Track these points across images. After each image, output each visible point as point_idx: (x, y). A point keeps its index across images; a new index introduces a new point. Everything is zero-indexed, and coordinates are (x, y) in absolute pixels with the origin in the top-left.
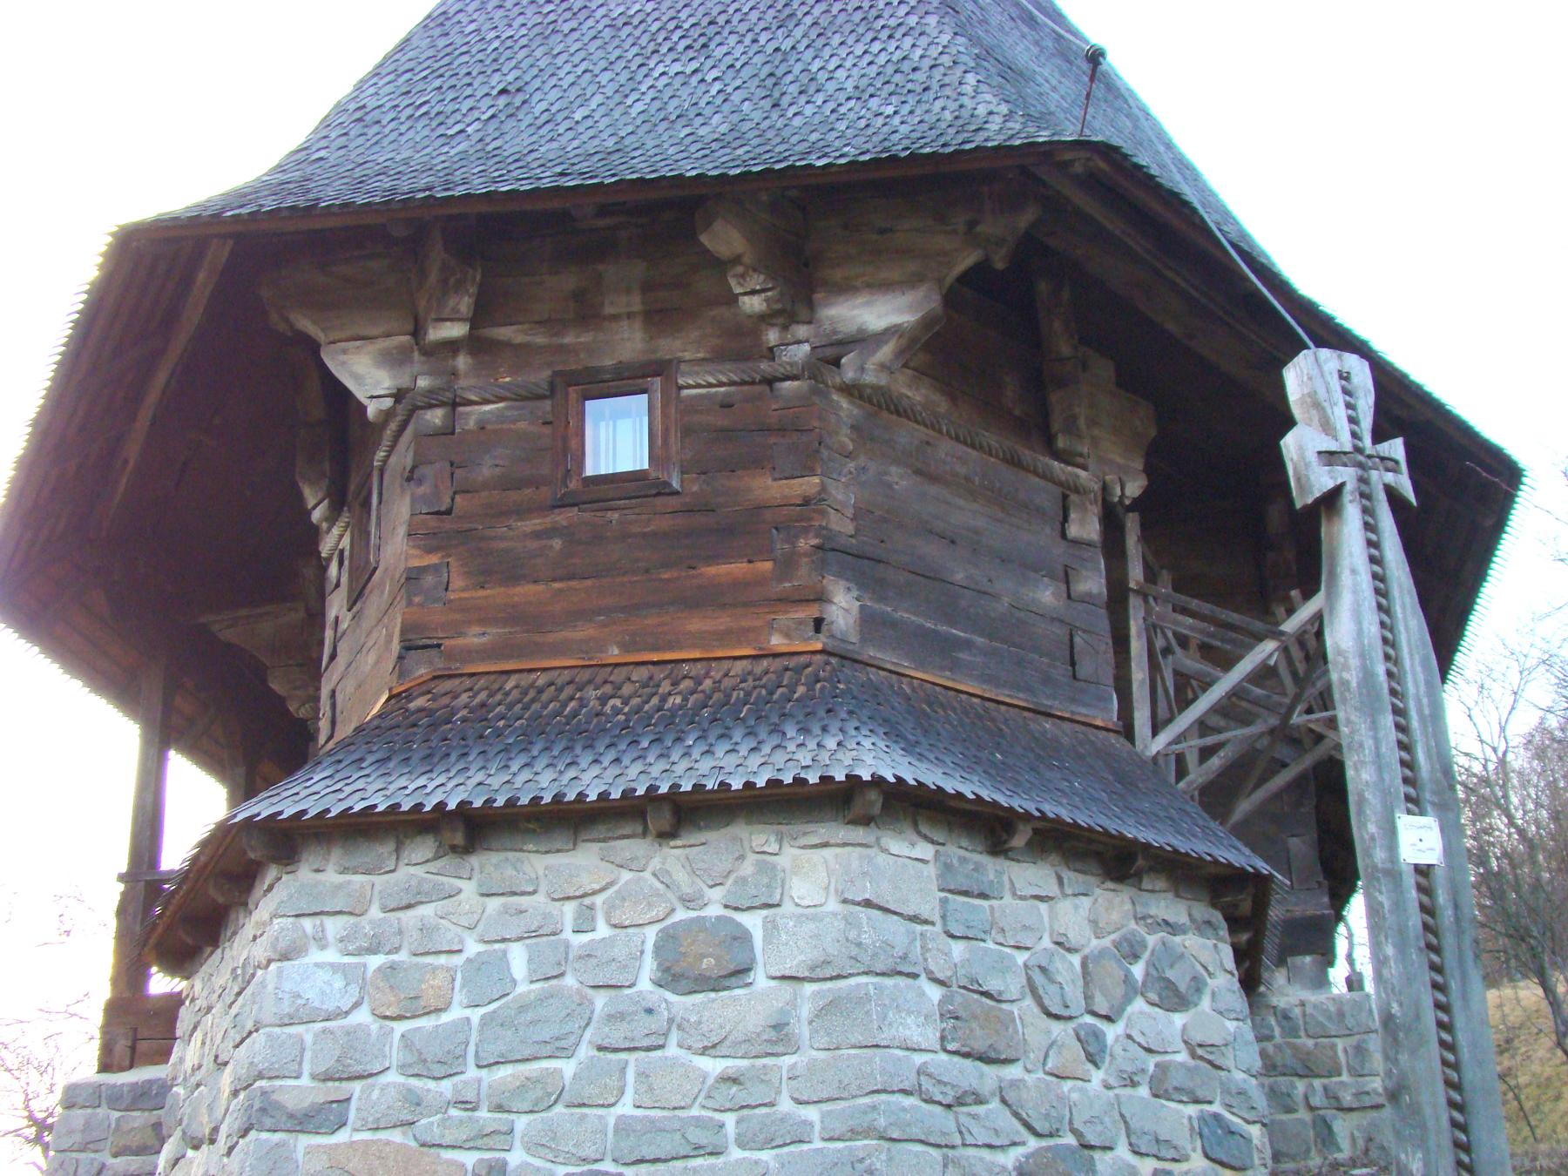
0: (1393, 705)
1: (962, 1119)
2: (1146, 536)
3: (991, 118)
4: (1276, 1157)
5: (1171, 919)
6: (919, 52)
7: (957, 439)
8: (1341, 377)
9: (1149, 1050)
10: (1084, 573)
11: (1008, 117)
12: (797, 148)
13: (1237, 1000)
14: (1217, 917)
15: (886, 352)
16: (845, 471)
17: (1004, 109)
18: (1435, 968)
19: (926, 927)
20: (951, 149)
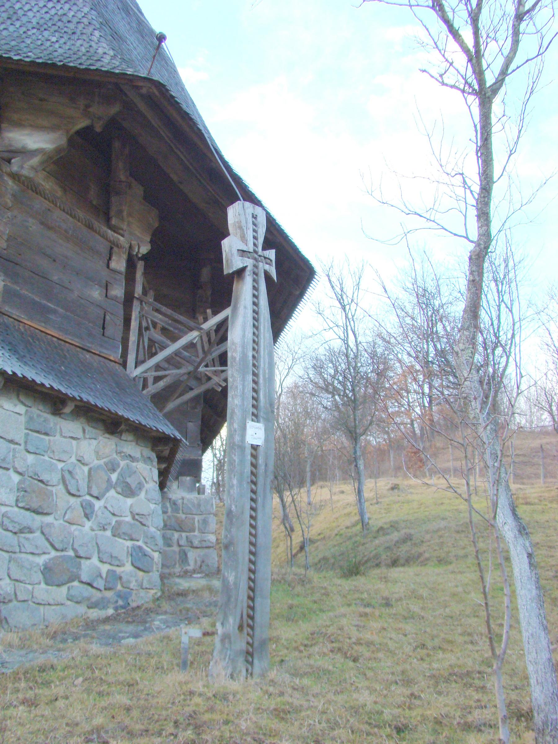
0: (253, 371)
1: (22, 540)
2: (145, 274)
3: (105, 56)
4: (163, 565)
5: (133, 454)
6: (72, 13)
7: (64, 210)
8: (253, 217)
9: (114, 514)
10: (115, 286)
11: (114, 57)
12: (3, 47)
13: (156, 493)
14: (153, 456)
15: (35, 161)
16: (6, 216)
17: (112, 53)
18: (253, 491)
19: (16, 446)
20: (84, 67)
